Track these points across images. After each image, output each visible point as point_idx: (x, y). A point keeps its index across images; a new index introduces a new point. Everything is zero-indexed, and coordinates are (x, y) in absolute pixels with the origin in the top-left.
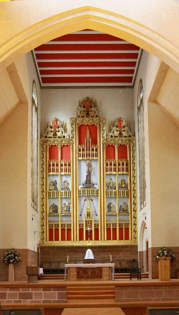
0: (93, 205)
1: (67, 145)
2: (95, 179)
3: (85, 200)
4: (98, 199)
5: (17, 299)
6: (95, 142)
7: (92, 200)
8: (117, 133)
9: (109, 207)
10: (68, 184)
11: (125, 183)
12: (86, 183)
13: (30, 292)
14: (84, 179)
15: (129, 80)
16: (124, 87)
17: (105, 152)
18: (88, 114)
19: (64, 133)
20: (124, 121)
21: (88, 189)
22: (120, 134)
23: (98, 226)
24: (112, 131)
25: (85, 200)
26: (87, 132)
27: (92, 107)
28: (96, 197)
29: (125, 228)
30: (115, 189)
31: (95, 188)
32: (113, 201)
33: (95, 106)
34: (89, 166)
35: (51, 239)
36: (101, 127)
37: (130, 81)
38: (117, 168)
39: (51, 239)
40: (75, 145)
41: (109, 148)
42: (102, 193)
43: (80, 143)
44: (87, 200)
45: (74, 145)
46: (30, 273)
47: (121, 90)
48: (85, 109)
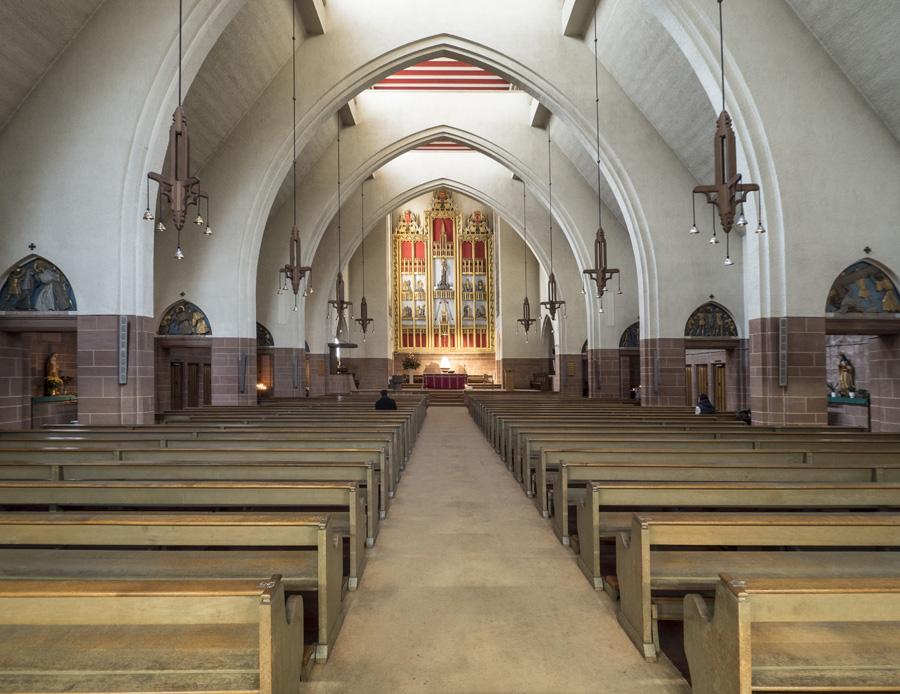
14: (439, 280)
22: (478, 230)
32: (469, 303)
35: (405, 345)
39: (405, 345)
41: (465, 245)
42: (458, 295)
43: (434, 240)
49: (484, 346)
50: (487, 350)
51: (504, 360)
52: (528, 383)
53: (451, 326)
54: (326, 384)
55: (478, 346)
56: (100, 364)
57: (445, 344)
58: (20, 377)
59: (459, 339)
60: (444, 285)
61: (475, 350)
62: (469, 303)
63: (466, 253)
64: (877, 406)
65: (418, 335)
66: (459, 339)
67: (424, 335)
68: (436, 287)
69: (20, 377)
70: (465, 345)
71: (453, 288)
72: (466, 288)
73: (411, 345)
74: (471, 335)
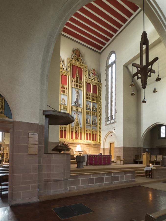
0: (79, 118)
1: (65, 75)
2: (82, 102)
3: (74, 114)
4: (81, 114)
5: (110, 181)
6: (81, 79)
7: (78, 114)
8: (92, 78)
9: (87, 119)
10: (65, 101)
11: (95, 108)
12: (76, 103)
13: (118, 175)
14: (74, 100)
15: (100, 48)
16: (96, 51)
17: (86, 86)
18: (77, 59)
19: (63, 66)
20: (96, 71)
21: (77, 107)
22: (94, 79)
23: (66, 129)
24: (90, 76)
25: (74, 114)
26: (77, 71)
27: (80, 56)
28: (81, 113)
29: (64, 131)
30: (91, 110)
31: (81, 107)
32: (89, 117)
33: (82, 56)
34: (78, 92)
35: (62, 137)
36: (85, 71)
37: (100, 50)
38: (94, 99)
39: (62, 137)
40: (69, 78)
41: (88, 85)
42: (84, 111)
43: (72, 77)
44: (76, 114)
45: (69, 76)
46: (119, 164)
47: (93, 52)
48: (76, 56)
49: (95, 140)
50: (97, 142)
51: (124, 147)
52: (133, 158)
53: (80, 128)
54: (40, 168)
55: (93, 140)
56: (39, 172)
57: (77, 138)
58: (14, 153)
59: (84, 136)
60: (77, 104)
61: (90, 142)
62: (89, 117)
63: (88, 89)
64: (65, 164)
65: (93, 134)
66: (84, 136)
67: (65, 131)
68: (73, 104)
69: (14, 153)
70: (87, 139)
71: (82, 106)
72: (88, 108)
73: (90, 139)
74: (90, 134)
